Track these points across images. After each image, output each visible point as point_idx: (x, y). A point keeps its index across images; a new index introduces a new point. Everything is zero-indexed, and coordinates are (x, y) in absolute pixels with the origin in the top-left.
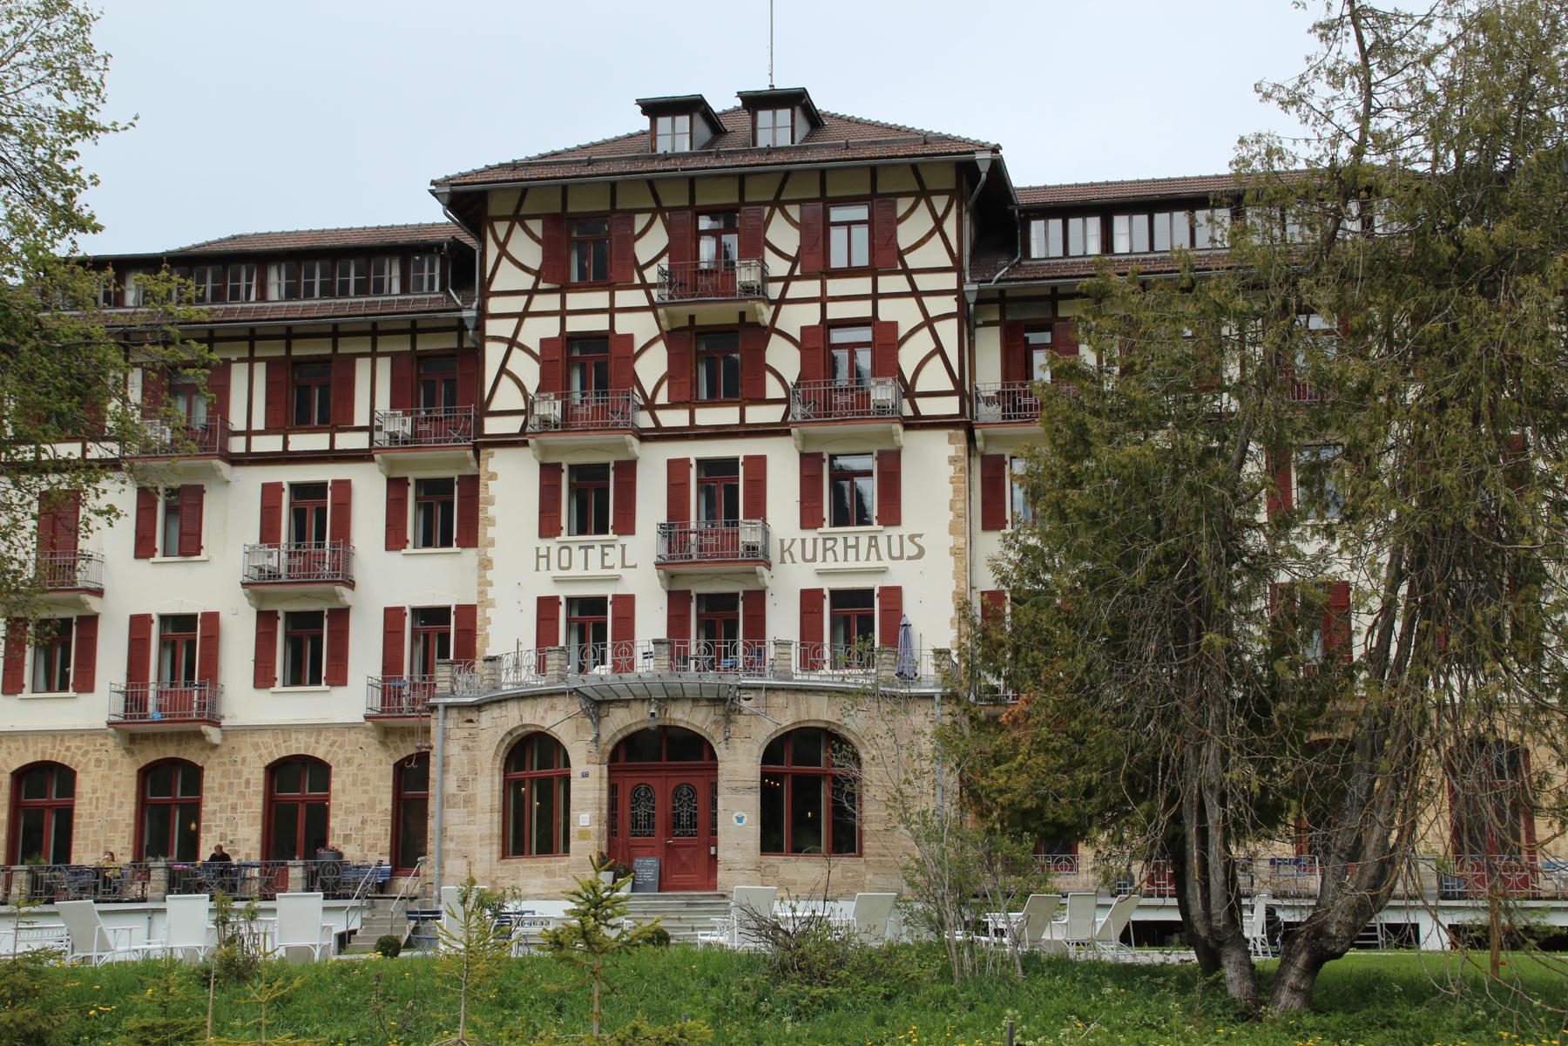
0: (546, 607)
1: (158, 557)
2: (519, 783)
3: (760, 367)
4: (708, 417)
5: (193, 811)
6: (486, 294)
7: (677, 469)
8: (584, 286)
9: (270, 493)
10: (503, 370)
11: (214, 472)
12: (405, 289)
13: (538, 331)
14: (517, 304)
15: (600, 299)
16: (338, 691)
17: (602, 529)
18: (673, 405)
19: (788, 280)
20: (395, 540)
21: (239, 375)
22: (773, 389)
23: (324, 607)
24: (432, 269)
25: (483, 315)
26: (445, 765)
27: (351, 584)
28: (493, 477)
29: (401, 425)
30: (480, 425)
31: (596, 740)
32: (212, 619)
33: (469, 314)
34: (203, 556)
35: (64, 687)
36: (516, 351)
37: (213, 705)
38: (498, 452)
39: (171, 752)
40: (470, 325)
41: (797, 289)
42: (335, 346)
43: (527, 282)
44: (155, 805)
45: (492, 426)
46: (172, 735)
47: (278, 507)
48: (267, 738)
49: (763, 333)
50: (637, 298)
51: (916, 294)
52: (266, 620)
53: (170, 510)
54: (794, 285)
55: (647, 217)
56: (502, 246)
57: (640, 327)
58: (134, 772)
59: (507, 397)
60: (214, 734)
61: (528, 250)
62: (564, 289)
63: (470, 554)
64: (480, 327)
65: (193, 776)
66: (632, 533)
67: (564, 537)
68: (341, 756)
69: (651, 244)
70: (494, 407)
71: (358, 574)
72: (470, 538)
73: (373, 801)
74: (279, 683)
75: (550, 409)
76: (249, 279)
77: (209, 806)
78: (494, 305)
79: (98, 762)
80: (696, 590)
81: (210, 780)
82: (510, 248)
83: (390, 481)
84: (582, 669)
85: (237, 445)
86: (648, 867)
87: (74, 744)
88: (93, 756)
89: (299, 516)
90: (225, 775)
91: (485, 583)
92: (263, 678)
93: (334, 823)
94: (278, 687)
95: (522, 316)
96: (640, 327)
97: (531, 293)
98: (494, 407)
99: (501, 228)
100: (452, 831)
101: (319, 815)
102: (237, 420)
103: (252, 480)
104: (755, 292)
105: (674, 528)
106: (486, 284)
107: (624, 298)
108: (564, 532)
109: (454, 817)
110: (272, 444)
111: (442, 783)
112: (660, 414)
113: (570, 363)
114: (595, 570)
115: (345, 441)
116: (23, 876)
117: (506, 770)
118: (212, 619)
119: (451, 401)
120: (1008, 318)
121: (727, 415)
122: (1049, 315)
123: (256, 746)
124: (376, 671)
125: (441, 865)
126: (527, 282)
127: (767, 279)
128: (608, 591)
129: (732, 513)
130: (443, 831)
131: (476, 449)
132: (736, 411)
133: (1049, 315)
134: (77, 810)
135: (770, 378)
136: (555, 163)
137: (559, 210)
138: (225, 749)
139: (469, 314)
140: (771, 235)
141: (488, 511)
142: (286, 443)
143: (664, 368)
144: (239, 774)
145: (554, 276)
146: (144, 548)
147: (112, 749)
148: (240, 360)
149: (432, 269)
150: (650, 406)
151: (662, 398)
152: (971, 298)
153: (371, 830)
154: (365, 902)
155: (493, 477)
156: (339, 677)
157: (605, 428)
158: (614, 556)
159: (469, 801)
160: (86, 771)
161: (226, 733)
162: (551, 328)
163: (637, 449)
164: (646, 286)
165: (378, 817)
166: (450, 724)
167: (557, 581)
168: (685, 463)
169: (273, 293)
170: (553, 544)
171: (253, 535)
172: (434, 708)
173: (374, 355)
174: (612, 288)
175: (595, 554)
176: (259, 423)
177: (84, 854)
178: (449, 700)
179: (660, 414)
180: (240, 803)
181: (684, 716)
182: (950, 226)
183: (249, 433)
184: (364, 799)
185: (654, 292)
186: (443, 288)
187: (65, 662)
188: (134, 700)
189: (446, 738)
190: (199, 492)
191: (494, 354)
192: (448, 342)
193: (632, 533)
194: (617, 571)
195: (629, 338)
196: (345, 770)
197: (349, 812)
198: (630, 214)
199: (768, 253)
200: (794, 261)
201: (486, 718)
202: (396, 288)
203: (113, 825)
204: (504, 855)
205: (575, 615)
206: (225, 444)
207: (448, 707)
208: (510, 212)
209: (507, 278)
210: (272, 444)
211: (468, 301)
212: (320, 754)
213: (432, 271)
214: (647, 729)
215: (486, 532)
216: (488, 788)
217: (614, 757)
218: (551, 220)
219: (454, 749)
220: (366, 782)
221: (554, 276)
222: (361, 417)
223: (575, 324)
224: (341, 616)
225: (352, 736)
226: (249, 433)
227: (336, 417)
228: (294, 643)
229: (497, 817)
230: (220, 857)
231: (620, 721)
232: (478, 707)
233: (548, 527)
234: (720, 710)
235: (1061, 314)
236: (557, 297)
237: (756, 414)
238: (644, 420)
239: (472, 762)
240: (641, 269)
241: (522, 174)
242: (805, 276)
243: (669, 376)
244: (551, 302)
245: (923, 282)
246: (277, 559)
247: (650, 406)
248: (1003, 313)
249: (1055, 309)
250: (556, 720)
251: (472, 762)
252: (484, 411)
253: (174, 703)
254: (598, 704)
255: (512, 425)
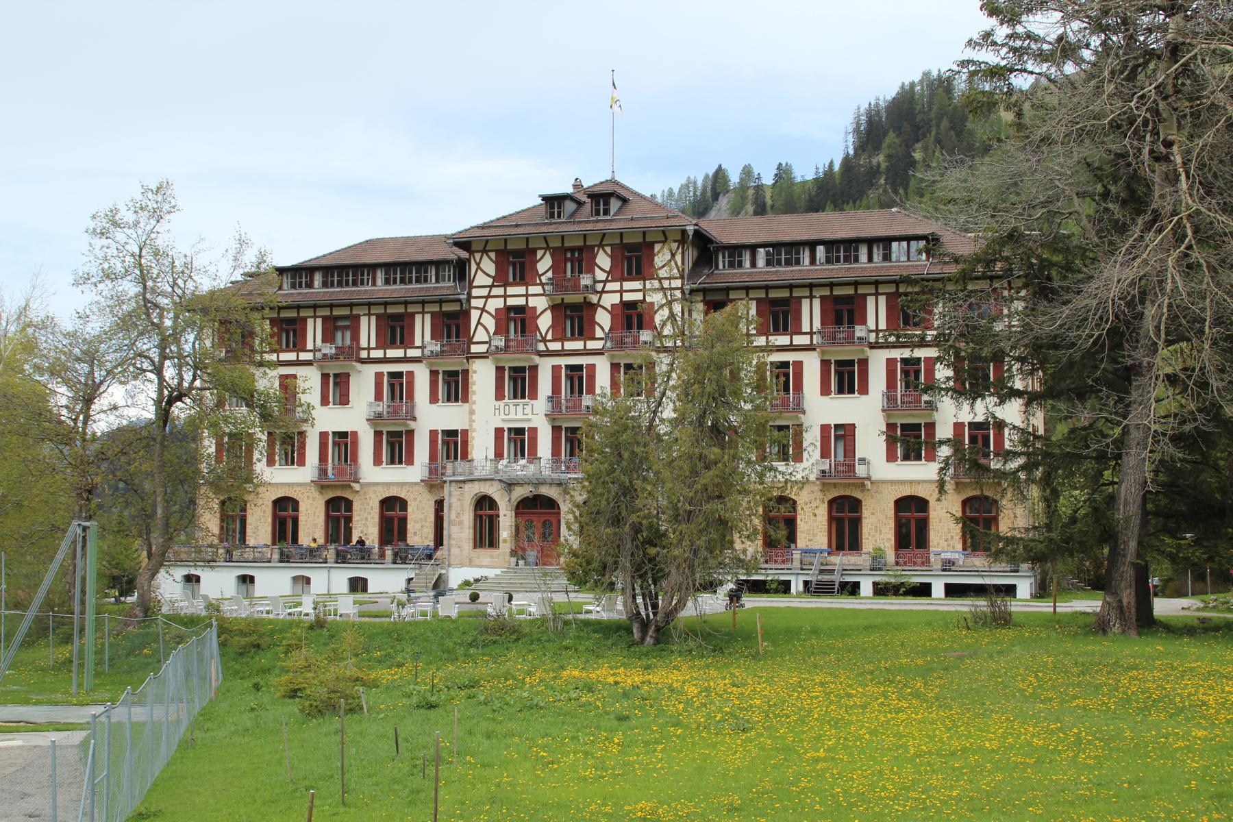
0: (499, 432)
1: (331, 405)
2: (481, 517)
3: (593, 323)
4: (570, 345)
5: (349, 519)
6: (471, 287)
7: (556, 369)
8: (515, 284)
9: (379, 376)
10: (479, 323)
11: (354, 367)
12: (437, 281)
13: (495, 304)
14: (485, 292)
15: (521, 290)
16: (410, 468)
17: (523, 397)
18: (554, 340)
19: (605, 282)
20: (434, 399)
21: (364, 321)
22: (599, 333)
23: (404, 429)
24: (449, 271)
25: (470, 297)
26: (450, 507)
27: (414, 419)
28: (475, 372)
29: (436, 347)
30: (469, 348)
31: (509, 500)
32: (355, 434)
33: (463, 297)
34: (350, 405)
35: (293, 463)
36: (484, 314)
37: (356, 473)
38: (477, 361)
39: (338, 493)
40: (464, 302)
41: (610, 286)
42: (406, 309)
43: (489, 281)
44: (333, 517)
45: (475, 349)
46: (339, 486)
47: (327, 443)
48: (380, 488)
49: (593, 307)
50: (538, 290)
51: (663, 289)
52: (378, 434)
53: (335, 384)
54: (608, 284)
55: (543, 251)
56: (478, 264)
57: (540, 303)
58: (323, 502)
59: (481, 335)
60: (356, 486)
61: (489, 266)
62: (506, 284)
63: (466, 405)
64: (468, 300)
65: (349, 504)
66: (536, 399)
67: (506, 400)
68: (412, 497)
69: (545, 264)
70: (474, 340)
71: (418, 414)
72: (466, 399)
73: (426, 517)
74: (384, 463)
75: (499, 342)
76: (368, 275)
77: (355, 518)
78: (475, 292)
79: (308, 497)
80: (564, 425)
81: (355, 506)
82: (481, 266)
83: (431, 372)
84: (970, 112)
85: (364, 354)
86: (532, 555)
87: (298, 489)
88: (306, 495)
89: (392, 386)
90: (362, 504)
91: (472, 421)
92: (377, 461)
93: (409, 527)
94: (384, 465)
95: (488, 297)
96: (540, 303)
97: (491, 287)
98: (474, 340)
99: (478, 256)
100: (453, 536)
101: (403, 521)
102: (363, 343)
103: (370, 371)
104: (591, 289)
105: (554, 398)
106: (471, 282)
107: (533, 289)
108: (507, 398)
109: (454, 529)
110: (378, 354)
111: (449, 515)
112: (548, 344)
113: (509, 319)
114: (520, 416)
115: (412, 353)
116: (277, 551)
117: (476, 509)
118: (355, 434)
119: (458, 336)
120: (707, 298)
121: (578, 345)
122: (725, 297)
123: (375, 492)
124: (426, 460)
125: (449, 551)
126: (489, 281)
127: (596, 282)
128: (526, 425)
129: (581, 392)
130: (450, 536)
131: (468, 359)
132: (582, 343)
133: (725, 297)
134: (300, 519)
135: (597, 328)
136: (497, 227)
137: (503, 248)
138: (362, 493)
139: (463, 297)
140: (598, 261)
141: (473, 388)
142: (385, 354)
143: (550, 323)
144: (368, 504)
145: (501, 279)
146: (325, 401)
147: (314, 492)
148: (364, 315)
149: (449, 271)
150: (544, 340)
151: (549, 337)
152: (687, 292)
153: (425, 530)
154: (417, 566)
155: (475, 372)
156: (410, 462)
157: (522, 352)
158: (528, 409)
159: (461, 523)
160: (303, 501)
161: (362, 486)
162: (500, 303)
163: (537, 360)
164: (542, 284)
165: (428, 525)
166: (452, 489)
167: (504, 420)
168: (560, 366)
169: (379, 281)
170: (501, 403)
171: (372, 397)
172: (445, 482)
173: (423, 313)
174: (527, 285)
175: (520, 408)
176: (373, 344)
177: (304, 540)
178: (452, 479)
179: (548, 344)
180: (369, 517)
181: (545, 491)
182: (678, 258)
183: (369, 349)
184: (422, 516)
185: (546, 287)
186: (454, 281)
187: (293, 452)
188: (323, 471)
189: (450, 495)
190: (348, 375)
191: (475, 315)
192: (455, 307)
193: (536, 399)
194: (530, 416)
195: (535, 308)
196: (414, 503)
197: (416, 522)
198: (534, 251)
199: (597, 269)
200: (608, 273)
201: (467, 487)
202: (433, 280)
203: (316, 525)
204: (475, 547)
205: (513, 436)
206: (358, 354)
207: (451, 481)
208: (481, 248)
209: (481, 279)
210: (378, 354)
211: (463, 289)
212: (402, 496)
213: (449, 272)
214: (527, 497)
215: (472, 397)
216: (468, 518)
217: (518, 507)
218: (498, 252)
219: (454, 500)
220: (423, 508)
221: (501, 279)
222: (418, 342)
223: (511, 302)
224: (411, 433)
225: (416, 488)
226: (369, 349)
227: (407, 341)
228: (391, 445)
229: (472, 531)
230: (361, 542)
231: (520, 493)
232: (464, 482)
233: (499, 396)
234: (561, 488)
235: (731, 297)
236: (503, 289)
237: (591, 345)
238: (541, 347)
239: (462, 506)
240: (540, 276)
241: (486, 232)
242: (613, 280)
243: (553, 326)
244: (500, 291)
245: (666, 284)
246: (382, 407)
247: (544, 340)
248: (704, 296)
249: (728, 295)
250: (493, 491)
251: (462, 506)
252: (470, 342)
253: (339, 472)
254: (510, 485)
255: (482, 348)
